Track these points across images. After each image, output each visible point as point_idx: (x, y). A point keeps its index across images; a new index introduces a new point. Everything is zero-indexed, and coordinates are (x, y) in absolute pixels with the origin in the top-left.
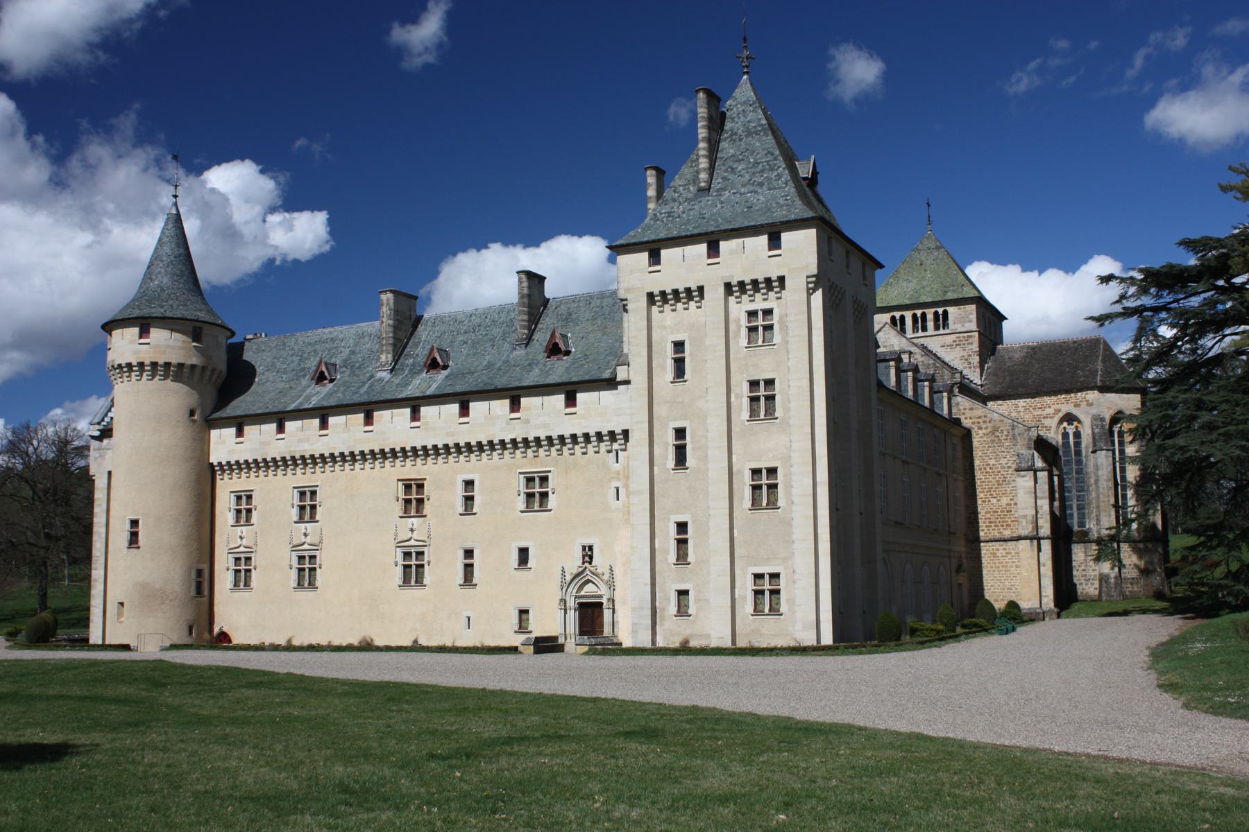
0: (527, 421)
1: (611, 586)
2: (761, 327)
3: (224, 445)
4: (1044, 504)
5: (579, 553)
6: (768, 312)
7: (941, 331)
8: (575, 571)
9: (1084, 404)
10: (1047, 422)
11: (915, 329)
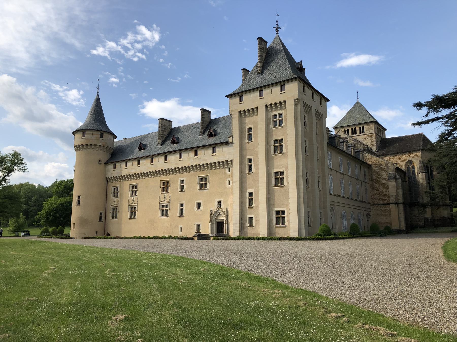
0: (200, 159)
1: (227, 215)
2: (278, 121)
3: (112, 172)
4: (401, 192)
5: (216, 204)
6: (281, 115)
7: (362, 134)
8: (215, 211)
9: (416, 157)
10: (402, 163)
11: (353, 134)
